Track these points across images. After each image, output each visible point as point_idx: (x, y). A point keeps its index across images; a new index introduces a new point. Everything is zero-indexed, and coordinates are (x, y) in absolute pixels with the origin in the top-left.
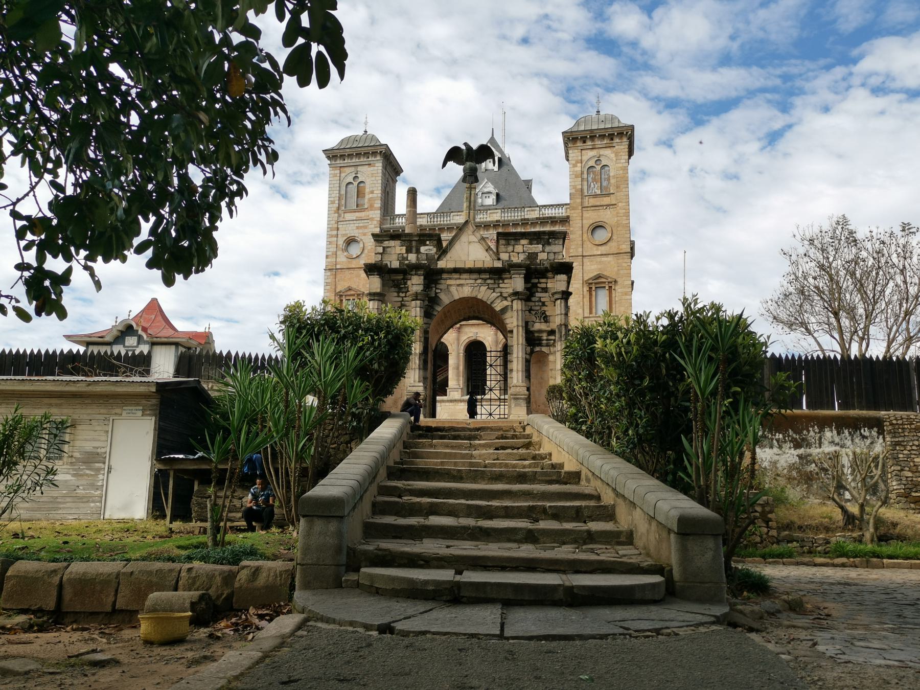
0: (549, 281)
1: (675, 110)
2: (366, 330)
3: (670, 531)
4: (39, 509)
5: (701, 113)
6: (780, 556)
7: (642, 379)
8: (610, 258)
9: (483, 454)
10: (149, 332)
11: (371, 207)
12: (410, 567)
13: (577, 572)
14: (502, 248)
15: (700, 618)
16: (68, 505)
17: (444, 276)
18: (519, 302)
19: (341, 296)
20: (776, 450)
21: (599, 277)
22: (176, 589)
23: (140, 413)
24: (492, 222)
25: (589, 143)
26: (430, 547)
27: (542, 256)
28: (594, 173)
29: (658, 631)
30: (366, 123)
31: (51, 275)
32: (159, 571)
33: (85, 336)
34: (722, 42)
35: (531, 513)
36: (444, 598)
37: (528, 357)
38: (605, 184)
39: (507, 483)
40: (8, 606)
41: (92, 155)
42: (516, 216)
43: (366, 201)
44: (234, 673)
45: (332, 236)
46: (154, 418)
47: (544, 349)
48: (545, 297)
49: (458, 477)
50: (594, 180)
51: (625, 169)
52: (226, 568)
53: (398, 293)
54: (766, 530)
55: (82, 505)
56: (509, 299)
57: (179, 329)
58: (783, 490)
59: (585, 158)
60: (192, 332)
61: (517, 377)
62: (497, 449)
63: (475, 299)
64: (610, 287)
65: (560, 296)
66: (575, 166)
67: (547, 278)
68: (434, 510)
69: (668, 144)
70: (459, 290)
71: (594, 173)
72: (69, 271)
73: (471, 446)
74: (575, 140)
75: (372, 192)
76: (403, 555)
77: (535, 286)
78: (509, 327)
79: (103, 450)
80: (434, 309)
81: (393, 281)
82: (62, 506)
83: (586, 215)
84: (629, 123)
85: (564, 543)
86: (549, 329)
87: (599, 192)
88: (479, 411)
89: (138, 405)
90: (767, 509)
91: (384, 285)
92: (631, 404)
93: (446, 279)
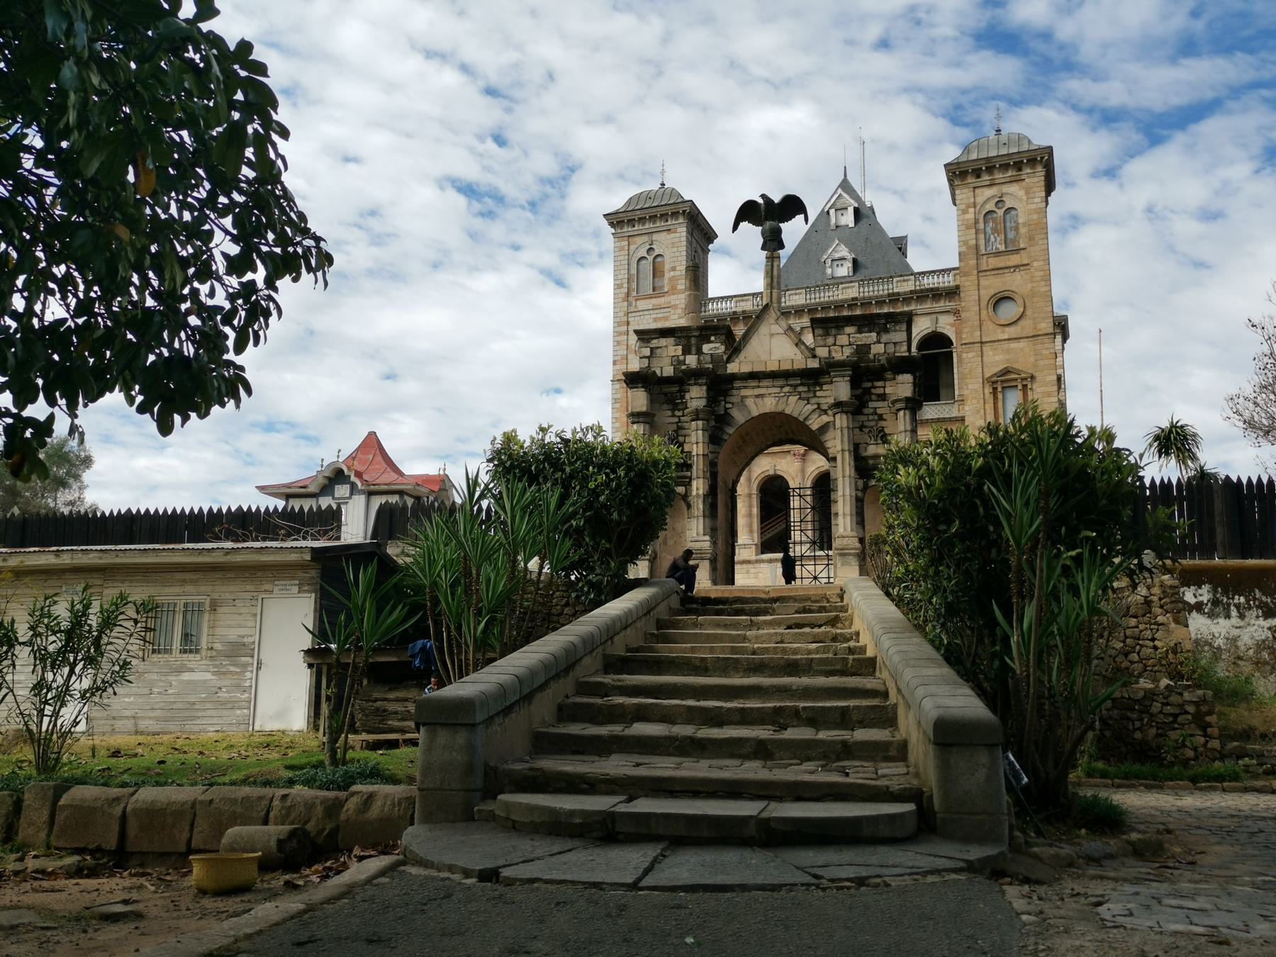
0: (888, 383)
1: (1116, 125)
2: (600, 467)
4: (172, 719)
5: (1158, 128)
6: (1220, 778)
7: (950, 523)
9: (763, 637)
10: (365, 477)
11: (673, 290)
12: (570, 793)
13: (799, 799)
15: (941, 863)
16: (209, 713)
17: (737, 384)
18: (844, 416)
20: (1235, 620)
21: (1007, 371)
22: (265, 822)
23: (296, 589)
24: (846, 301)
25: (986, 177)
26: (617, 766)
27: (877, 349)
28: (994, 220)
29: (861, 882)
30: (663, 172)
31: (31, 422)
32: (246, 799)
33: (284, 486)
34: (1179, 21)
35: (777, 718)
36: (595, 834)
37: (860, 494)
38: (1011, 235)
39: (771, 676)
40: (60, 845)
41: (184, 253)
42: (881, 290)
43: (666, 281)
44: (249, 931)
45: (620, 334)
48: (882, 407)
49: (701, 668)
50: (995, 230)
51: (1043, 212)
52: (331, 794)
53: (673, 411)
54: (1202, 740)
55: (225, 712)
56: (830, 412)
57: (407, 471)
58: (1248, 680)
59: (980, 200)
60: (422, 476)
61: (843, 525)
62: (789, 627)
63: (782, 414)
64: (1025, 386)
65: (903, 405)
66: (965, 212)
67: (885, 380)
68: (642, 715)
69: (1110, 173)
70: (760, 402)
71: (994, 220)
72: (51, 418)
73: (752, 625)
75: (674, 269)
76: (561, 775)
77: (868, 392)
78: (831, 452)
79: (251, 640)
80: (723, 431)
81: (666, 394)
82: (200, 714)
83: (984, 282)
84: (1045, 144)
85: (809, 759)
87: (1002, 248)
88: (798, 574)
89: (293, 578)
90: (1204, 709)
91: (652, 401)
92: (936, 561)
93: (739, 388)
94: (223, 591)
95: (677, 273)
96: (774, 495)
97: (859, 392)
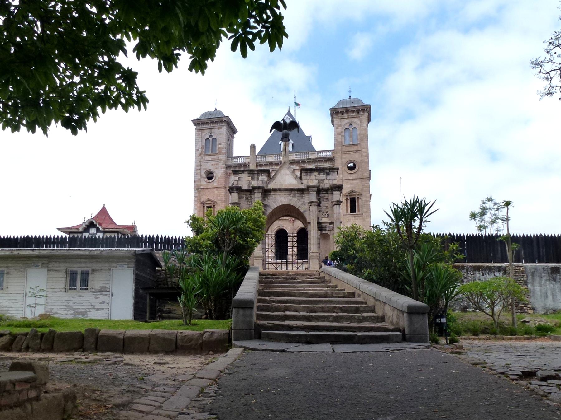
3: (403, 312)
8: (358, 181)
11: (220, 153)
14: (303, 177)
17: (272, 193)
19: (204, 204)
25: (345, 115)
45: (197, 170)
46: (133, 269)
47: (327, 232)
59: (343, 123)
66: (337, 128)
74: (337, 113)
75: (220, 144)
86: (330, 221)
94: (97, 266)
95: (222, 146)
96: (281, 235)
97: (319, 198)
